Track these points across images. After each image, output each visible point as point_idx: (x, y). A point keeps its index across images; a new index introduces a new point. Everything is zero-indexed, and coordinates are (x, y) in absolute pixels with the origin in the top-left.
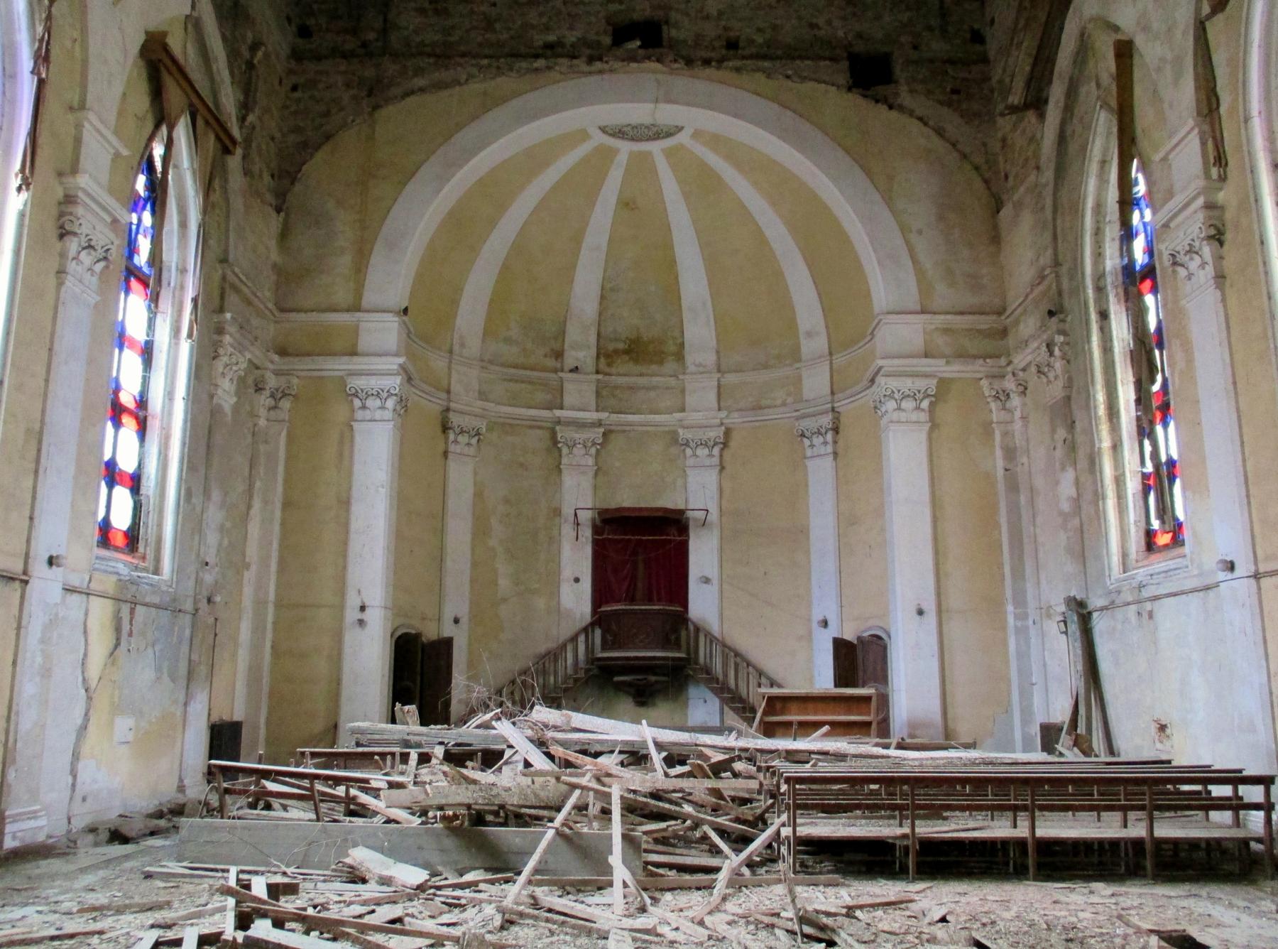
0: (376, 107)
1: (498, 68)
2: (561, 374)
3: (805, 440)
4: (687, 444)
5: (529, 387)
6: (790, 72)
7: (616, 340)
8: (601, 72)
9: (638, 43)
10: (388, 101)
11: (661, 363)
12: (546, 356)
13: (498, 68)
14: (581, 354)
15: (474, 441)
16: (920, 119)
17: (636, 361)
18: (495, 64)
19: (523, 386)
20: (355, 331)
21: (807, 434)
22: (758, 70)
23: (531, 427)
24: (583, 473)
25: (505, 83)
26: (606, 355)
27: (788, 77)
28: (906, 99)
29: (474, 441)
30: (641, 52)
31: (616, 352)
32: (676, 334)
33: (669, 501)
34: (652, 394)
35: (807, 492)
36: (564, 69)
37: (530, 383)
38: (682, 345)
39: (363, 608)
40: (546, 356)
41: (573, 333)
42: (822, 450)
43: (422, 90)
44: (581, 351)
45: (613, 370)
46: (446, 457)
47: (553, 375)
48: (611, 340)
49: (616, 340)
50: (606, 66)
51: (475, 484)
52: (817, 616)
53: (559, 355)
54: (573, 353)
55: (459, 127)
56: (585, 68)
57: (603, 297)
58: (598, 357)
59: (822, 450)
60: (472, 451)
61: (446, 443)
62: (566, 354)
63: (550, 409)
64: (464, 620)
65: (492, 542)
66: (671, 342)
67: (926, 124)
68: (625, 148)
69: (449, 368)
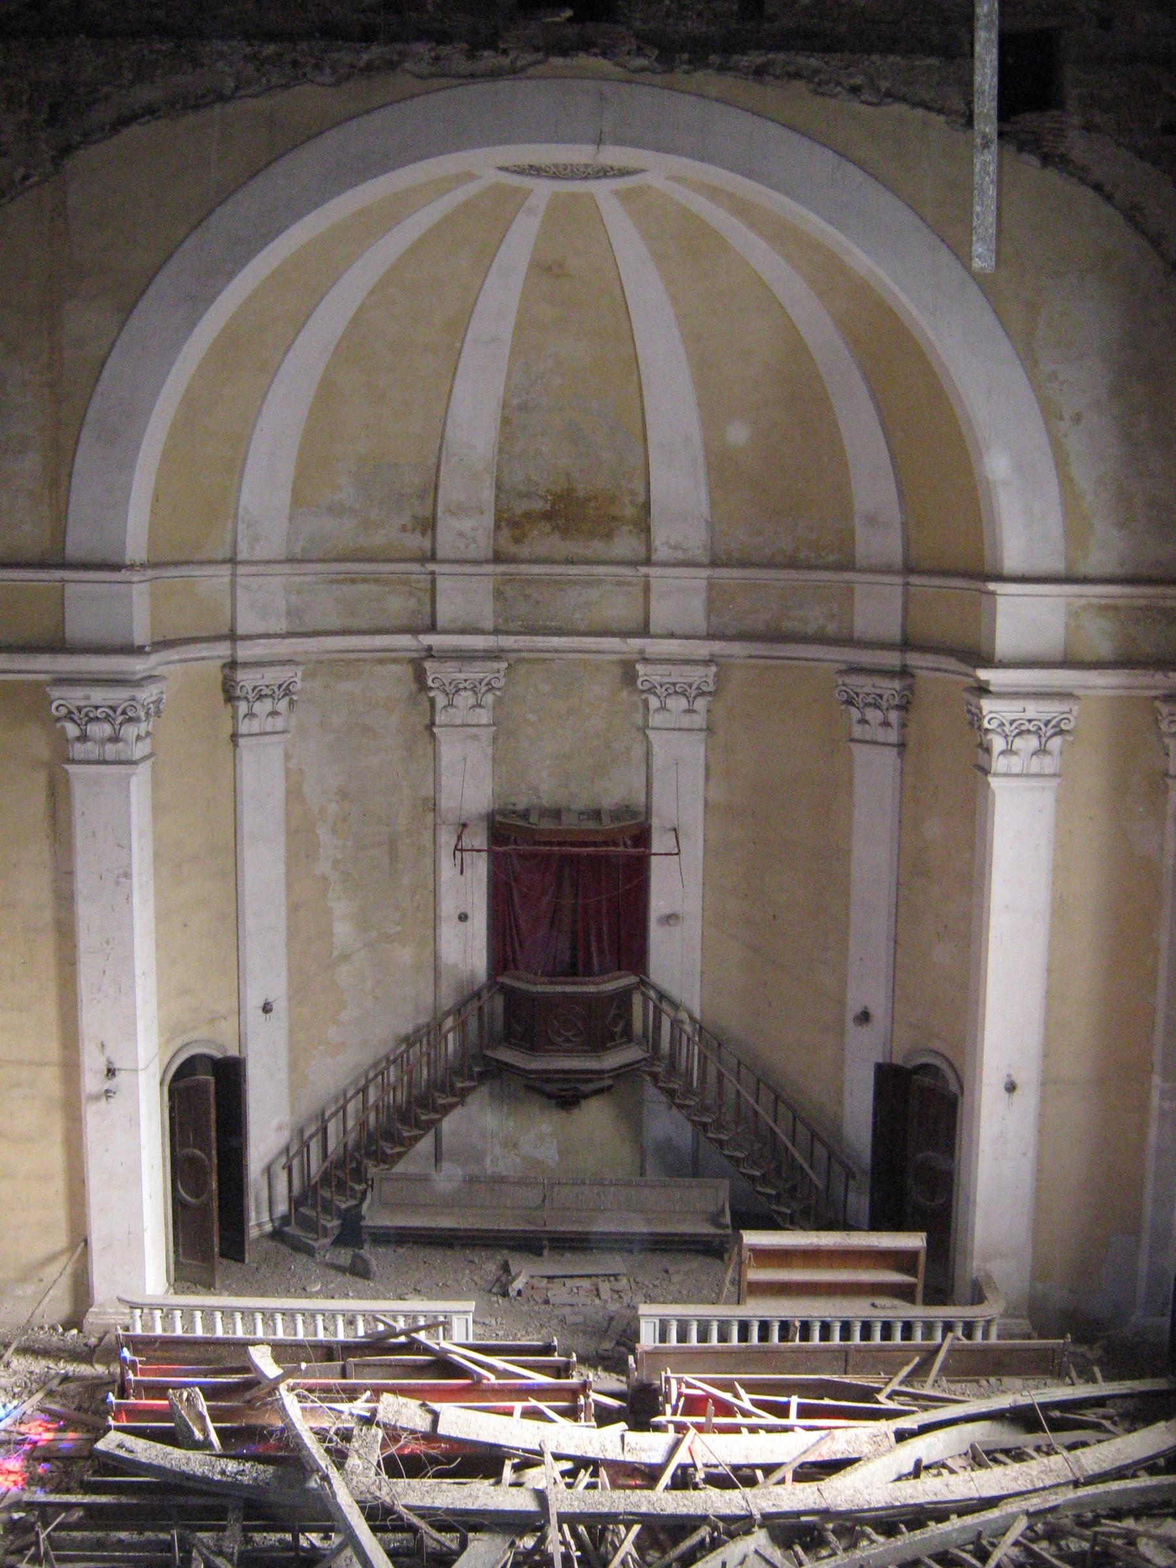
0: (66, 150)
1: (295, 64)
2: (431, 567)
3: (853, 710)
4: (651, 690)
5: (374, 588)
6: (858, 81)
7: (528, 495)
8: (495, 74)
9: (568, 13)
10: (87, 138)
11: (609, 536)
12: (404, 529)
13: (295, 64)
14: (466, 524)
15: (282, 705)
16: (1097, 187)
17: (565, 533)
18: (287, 57)
19: (364, 587)
20: (32, 1480)
21: (859, 701)
22: (797, 75)
23: (381, 662)
24: (475, 738)
25: (308, 98)
26: (512, 523)
27: (855, 90)
28: (1077, 145)
29: (282, 705)
30: (571, 31)
31: (528, 515)
32: (638, 485)
33: (616, 789)
34: (594, 594)
35: (850, 795)
36: (424, 68)
37: (377, 581)
38: (646, 507)
39: (111, 1072)
40: (404, 529)
41: (452, 489)
42: (881, 735)
43: (151, 111)
44: (466, 527)
45: (524, 551)
46: (236, 745)
47: (416, 567)
48: (521, 496)
49: (528, 495)
50: (506, 61)
51: (288, 772)
52: (854, 1006)
53: (429, 525)
54: (456, 524)
55: (224, 194)
56: (461, 65)
57: (506, 421)
58: (498, 527)
59: (881, 735)
60: (279, 723)
61: (234, 717)
62: (441, 525)
63: (415, 631)
64: (280, 1007)
65: (323, 867)
66: (626, 500)
67: (1109, 198)
68: (542, 190)
69: (233, 585)
